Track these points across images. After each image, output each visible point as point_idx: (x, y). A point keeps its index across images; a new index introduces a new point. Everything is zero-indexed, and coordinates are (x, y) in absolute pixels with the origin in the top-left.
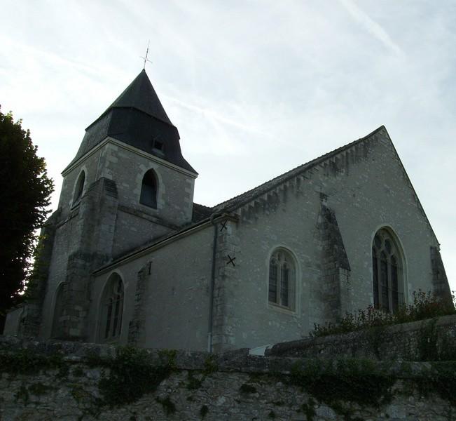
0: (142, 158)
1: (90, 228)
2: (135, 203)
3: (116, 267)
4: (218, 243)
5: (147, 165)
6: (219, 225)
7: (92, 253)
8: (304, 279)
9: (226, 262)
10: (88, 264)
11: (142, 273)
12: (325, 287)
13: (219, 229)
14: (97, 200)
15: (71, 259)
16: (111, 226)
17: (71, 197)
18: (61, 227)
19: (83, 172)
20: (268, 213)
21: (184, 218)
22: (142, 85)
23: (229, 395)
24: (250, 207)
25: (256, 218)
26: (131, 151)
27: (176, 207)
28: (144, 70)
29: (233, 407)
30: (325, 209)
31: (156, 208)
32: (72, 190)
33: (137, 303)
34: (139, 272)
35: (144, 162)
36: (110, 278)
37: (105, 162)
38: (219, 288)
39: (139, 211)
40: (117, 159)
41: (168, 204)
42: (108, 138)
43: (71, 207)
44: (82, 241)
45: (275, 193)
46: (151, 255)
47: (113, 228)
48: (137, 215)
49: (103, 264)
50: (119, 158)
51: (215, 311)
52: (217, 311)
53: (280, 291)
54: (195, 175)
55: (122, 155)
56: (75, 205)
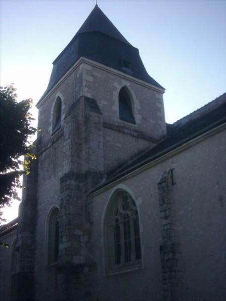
1: (77, 149)
2: (116, 119)
3: (120, 182)
5: (120, 83)
7: (84, 172)
10: (81, 185)
11: (164, 184)
14: (81, 119)
15: (63, 180)
16: (99, 142)
17: (49, 125)
18: (44, 154)
19: (59, 99)
26: (102, 69)
27: (152, 121)
28: (97, 6)
31: (134, 123)
32: (50, 117)
33: (167, 221)
34: (160, 183)
35: (118, 81)
36: (113, 194)
37: (82, 82)
39: (120, 126)
40: (92, 78)
41: (144, 119)
42: (82, 58)
43: (51, 133)
44: (72, 161)
46: (170, 160)
47: (101, 144)
48: (119, 131)
50: (94, 76)
54: (163, 90)
55: (98, 74)
56: (56, 129)
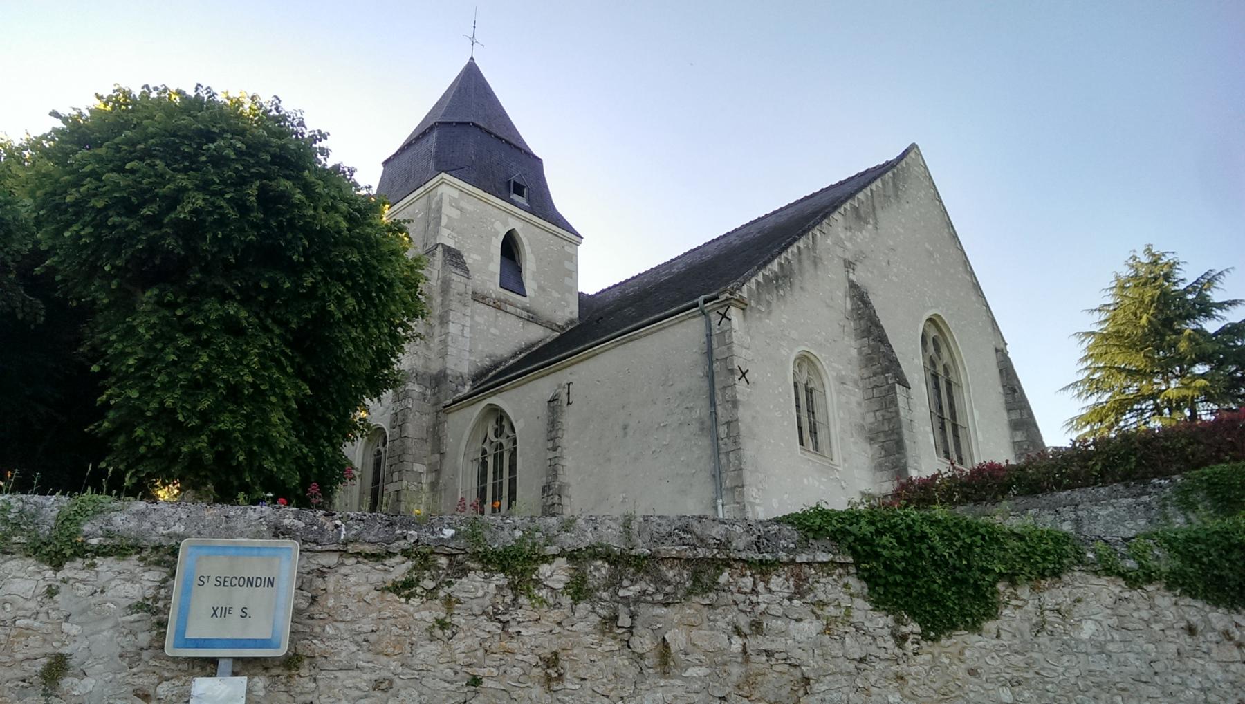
0: (497, 211)
2: (492, 285)
3: (494, 394)
4: (715, 345)
5: (505, 224)
6: (713, 315)
8: (844, 406)
9: (737, 377)
12: (870, 418)
13: (714, 323)
20: (781, 292)
21: (567, 311)
22: (471, 85)
23: (1098, 617)
24: (758, 283)
25: (769, 303)
29: (1113, 641)
30: (853, 285)
38: (728, 423)
41: (541, 288)
45: (787, 259)
48: (499, 308)
49: (457, 391)
50: (461, 209)
51: (724, 460)
52: (729, 462)
53: (810, 431)
